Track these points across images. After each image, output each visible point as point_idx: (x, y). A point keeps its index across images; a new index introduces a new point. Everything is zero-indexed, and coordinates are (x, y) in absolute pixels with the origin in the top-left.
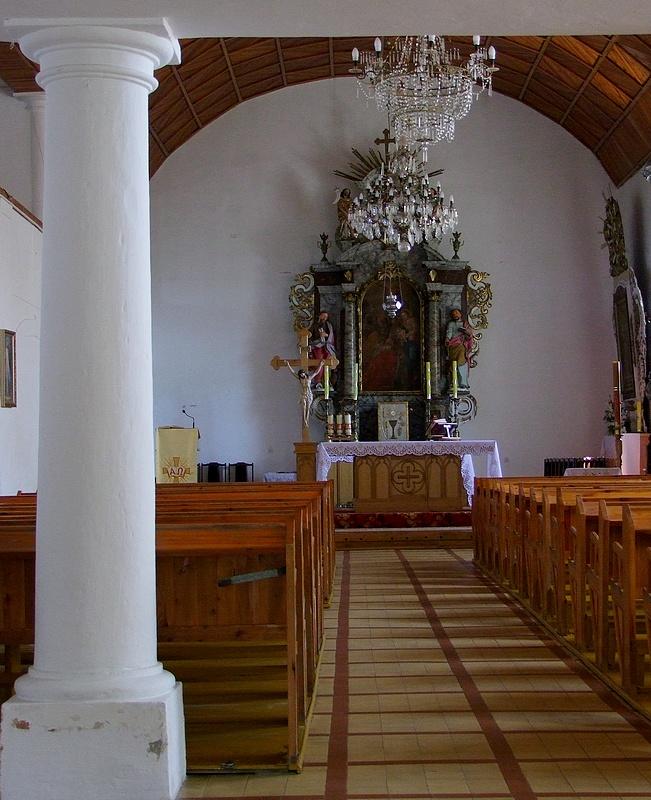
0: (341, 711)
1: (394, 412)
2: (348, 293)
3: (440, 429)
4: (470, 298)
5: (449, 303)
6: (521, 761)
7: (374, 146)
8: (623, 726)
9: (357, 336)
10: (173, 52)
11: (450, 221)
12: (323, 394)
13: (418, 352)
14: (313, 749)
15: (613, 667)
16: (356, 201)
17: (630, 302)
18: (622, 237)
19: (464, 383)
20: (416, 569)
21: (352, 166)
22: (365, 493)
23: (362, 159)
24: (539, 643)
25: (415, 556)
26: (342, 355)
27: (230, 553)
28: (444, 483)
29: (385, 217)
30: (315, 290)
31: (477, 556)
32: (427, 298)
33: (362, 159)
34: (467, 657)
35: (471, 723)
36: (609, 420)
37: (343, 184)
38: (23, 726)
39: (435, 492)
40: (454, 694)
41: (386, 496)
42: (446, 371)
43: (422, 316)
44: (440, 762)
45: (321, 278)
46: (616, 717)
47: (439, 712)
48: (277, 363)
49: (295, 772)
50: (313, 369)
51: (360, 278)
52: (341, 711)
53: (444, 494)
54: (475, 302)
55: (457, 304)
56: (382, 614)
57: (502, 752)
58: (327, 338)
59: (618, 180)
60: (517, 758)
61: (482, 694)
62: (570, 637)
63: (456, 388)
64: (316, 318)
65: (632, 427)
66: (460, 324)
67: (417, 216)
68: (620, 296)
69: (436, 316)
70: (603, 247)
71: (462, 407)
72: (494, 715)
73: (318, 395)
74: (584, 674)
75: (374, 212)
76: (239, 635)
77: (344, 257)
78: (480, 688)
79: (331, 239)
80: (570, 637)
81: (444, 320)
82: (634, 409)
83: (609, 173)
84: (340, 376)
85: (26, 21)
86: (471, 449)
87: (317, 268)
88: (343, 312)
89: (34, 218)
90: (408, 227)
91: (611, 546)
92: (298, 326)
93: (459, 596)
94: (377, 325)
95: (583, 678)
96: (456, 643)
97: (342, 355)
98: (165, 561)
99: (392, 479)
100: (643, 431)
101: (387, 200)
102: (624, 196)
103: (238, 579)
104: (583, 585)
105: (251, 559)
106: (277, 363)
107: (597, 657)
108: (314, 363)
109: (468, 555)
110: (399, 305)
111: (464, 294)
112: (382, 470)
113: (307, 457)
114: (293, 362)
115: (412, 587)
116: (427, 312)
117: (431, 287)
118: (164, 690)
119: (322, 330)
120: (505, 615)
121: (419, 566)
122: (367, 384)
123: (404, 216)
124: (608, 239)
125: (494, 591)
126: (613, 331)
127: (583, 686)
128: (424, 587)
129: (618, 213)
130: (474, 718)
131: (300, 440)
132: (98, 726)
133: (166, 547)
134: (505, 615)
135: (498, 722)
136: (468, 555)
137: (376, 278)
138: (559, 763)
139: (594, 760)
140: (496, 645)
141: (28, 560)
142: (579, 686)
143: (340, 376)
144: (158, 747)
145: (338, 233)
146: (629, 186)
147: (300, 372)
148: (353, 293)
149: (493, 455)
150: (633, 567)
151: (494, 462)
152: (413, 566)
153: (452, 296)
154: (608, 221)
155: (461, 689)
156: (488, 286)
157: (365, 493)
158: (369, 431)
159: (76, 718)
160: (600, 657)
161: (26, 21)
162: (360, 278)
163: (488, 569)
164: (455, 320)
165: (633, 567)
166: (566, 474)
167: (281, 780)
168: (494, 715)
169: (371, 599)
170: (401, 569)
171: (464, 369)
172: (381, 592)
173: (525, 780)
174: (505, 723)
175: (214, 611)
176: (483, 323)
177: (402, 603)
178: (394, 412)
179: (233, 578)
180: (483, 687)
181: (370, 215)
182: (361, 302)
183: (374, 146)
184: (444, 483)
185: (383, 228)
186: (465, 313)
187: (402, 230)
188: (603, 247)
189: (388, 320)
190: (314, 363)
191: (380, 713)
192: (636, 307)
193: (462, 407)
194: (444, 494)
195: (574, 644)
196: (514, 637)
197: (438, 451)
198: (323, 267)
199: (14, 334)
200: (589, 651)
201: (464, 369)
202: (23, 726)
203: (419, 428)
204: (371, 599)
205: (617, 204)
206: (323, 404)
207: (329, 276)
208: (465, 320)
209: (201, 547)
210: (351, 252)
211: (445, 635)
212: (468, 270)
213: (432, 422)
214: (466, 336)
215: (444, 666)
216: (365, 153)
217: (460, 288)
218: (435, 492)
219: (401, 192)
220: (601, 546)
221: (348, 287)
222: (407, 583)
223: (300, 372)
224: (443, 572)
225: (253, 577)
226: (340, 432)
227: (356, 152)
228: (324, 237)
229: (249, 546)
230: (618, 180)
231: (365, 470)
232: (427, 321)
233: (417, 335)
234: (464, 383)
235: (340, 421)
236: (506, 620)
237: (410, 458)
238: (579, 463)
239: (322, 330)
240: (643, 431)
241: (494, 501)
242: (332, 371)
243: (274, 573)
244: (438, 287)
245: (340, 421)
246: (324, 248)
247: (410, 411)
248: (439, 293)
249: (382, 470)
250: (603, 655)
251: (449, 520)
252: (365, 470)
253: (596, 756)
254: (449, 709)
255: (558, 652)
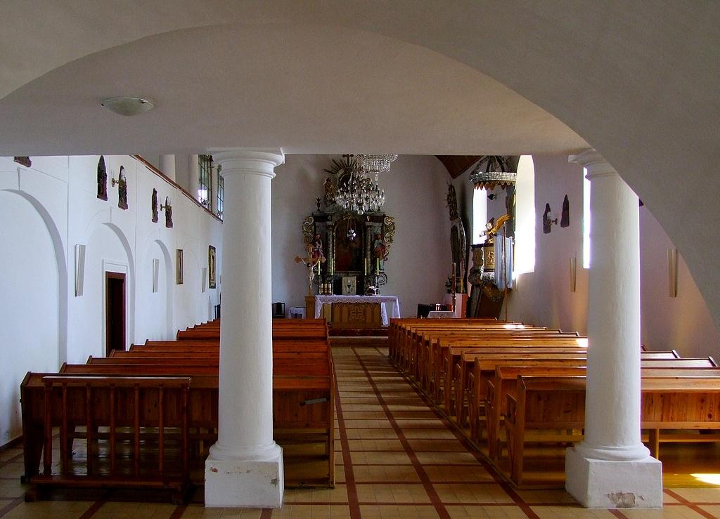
0: (346, 451)
1: (350, 281)
2: (329, 226)
3: (372, 291)
4: (385, 229)
5: (375, 231)
6: (434, 483)
7: (342, 158)
8: (474, 461)
9: (333, 246)
10: (281, 159)
11: (382, 200)
12: (318, 272)
13: (361, 254)
14: (339, 475)
15: (466, 426)
16: (339, 191)
17: (459, 232)
18: (456, 203)
19: (381, 268)
20: (365, 360)
21: (332, 167)
22: (337, 318)
23: (337, 164)
24: (427, 408)
25: (363, 352)
26: (326, 255)
27: (304, 390)
28: (373, 315)
29: (353, 199)
30: (314, 224)
31: (390, 353)
32: (366, 228)
33: (337, 164)
34: (398, 417)
35: (405, 459)
36: (448, 286)
37: (327, 175)
38: (215, 470)
39: (369, 320)
40: (393, 440)
41: (347, 321)
42: (374, 263)
43: (363, 237)
44: (393, 483)
45: (317, 218)
46: (470, 456)
47: (389, 451)
48: (298, 260)
49: (333, 488)
50: (314, 263)
51: (335, 219)
52: (346, 451)
53: (373, 320)
54: (388, 231)
55: (379, 232)
56: (351, 389)
57: (423, 477)
58: (320, 246)
59: (454, 175)
60: (432, 481)
61: (408, 441)
62: (442, 406)
63: (378, 271)
64: (314, 237)
65: (458, 290)
66: (380, 241)
67: (367, 199)
68: (454, 230)
69: (369, 237)
70: (446, 207)
71: (381, 279)
72: (417, 454)
73: (315, 272)
74: (450, 428)
75: (347, 196)
76: (307, 426)
77: (328, 209)
78: (407, 437)
79: (322, 201)
80: (442, 406)
81: (373, 239)
82: (460, 282)
83: (450, 172)
84: (325, 266)
85: (217, 149)
86: (385, 300)
87: (315, 214)
88: (327, 234)
89: (191, 196)
90: (363, 203)
91: (467, 374)
92: (306, 240)
93: (386, 378)
94: (342, 240)
95: (451, 431)
96: (391, 407)
97: (326, 255)
98: (276, 393)
99: (349, 314)
100: (463, 293)
101: (353, 191)
102: (457, 183)
103: (308, 402)
104: (463, 398)
105: (312, 394)
106: (298, 260)
107: (458, 419)
108: (315, 260)
109: (386, 352)
110: (354, 235)
111: (382, 227)
112: (345, 309)
113: (310, 303)
114: (305, 260)
115: (363, 372)
116: (365, 235)
117: (367, 224)
118: (275, 454)
119: (317, 243)
120: (409, 391)
121: (365, 358)
122: (338, 267)
123: (361, 198)
124: (449, 203)
125: (402, 375)
126: (450, 245)
127: (452, 437)
128: (369, 372)
129: (454, 192)
130: (408, 457)
131: (308, 295)
132: (248, 472)
133: (278, 387)
134: (409, 391)
135: (418, 458)
136: (386, 352)
137: (342, 219)
138: (465, 506)
139: (466, 483)
140: (407, 409)
141: (215, 392)
142: (450, 436)
143: (325, 266)
144: (275, 482)
145: (325, 197)
146: (459, 178)
147: (308, 264)
148: (332, 226)
149: (396, 303)
150: (479, 385)
151: (396, 307)
152: (362, 358)
153: (377, 227)
154: (449, 195)
155: (397, 437)
156: (393, 223)
157: (337, 318)
158: (338, 290)
159: (239, 468)
160: (459, 421)
161: (217, 149)
162: (335, 219)
163: (396, 362)
164: (378, 239)
165: (479, 385)
166: (429, 316)
167: (327, 492)
168: (417, 454)
169: (346, 379)
170: (356, 360)
171: (382, 262)
172: (351, 375)
173: (437, 496)
174: (423, 459)
175: (296, 415)
176: (391, 241)
177: (357, 382)
178: (350, 281)
179: (306, 402)
180: (408, 436)
181: (345, 197)
182: (335, 230)
183: (342, 158)
184: (373, 315)
185: (351, 203)
186: (383, 235)
187: (360, 205)
188: (446, 207)
189: (348, 240)
190: (315, 260)
191: (364, 451)
192: (462, 236)
193: (381, 279)
194: (373, 320)
195: (445, 411)
196: (418, 405)
197: (370, 301)
198: (318, 214)
199: (182, 250)
200: (452, 415)
201: (382, 262)
202: (215, 470)
203: (361, 291)
204: (346, 379)
205: (454, 188)
206: (317, 276)
207: (321, 218)
208: (382, 239)
209: (293, 387)
210: (331, 207)
211: (384, 402)
212: (384, 216)
213: (368, 287)
214: (383, 247)
215: (386, 422)
216: (338, 162)
217: (381, 224)
218: (369, 320)
219: (360, 187)
220: (461, 372)
221: (329, 223)
222: (359, 369)
223: (308, 264)
224: (375, 362)
225: (314, 401)
226: (326, 292)
227: (334, 161)
228: (319, 200)
229: (313, 387)
230: (454, 175)
231: (337, 309)
232: (365, 239)
233: (361, 245)
234: (381, 268)
235: (326, 287)
236: (411, 394)
237: (358, 304)
238: (433, 308)
239: (317, 243)
240: (463, 293)
241: (401, 332)
242: (321, 263)
243: (325, 400)
244: (371, 223)
245: (326, 287)
246: (319, 205)
247: (357, 282)
248: (371, 226)
249: (345, 309)
250: (461, 420)
251: (375, 333)
252: (337, 309)
253: (467, 480)
254: (396, 450)
255: (438, 415)
